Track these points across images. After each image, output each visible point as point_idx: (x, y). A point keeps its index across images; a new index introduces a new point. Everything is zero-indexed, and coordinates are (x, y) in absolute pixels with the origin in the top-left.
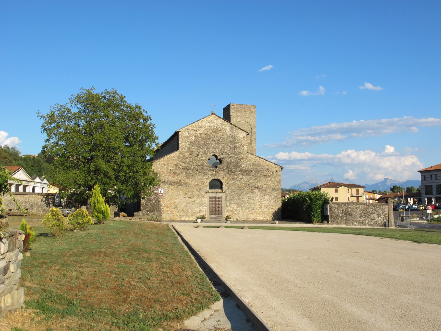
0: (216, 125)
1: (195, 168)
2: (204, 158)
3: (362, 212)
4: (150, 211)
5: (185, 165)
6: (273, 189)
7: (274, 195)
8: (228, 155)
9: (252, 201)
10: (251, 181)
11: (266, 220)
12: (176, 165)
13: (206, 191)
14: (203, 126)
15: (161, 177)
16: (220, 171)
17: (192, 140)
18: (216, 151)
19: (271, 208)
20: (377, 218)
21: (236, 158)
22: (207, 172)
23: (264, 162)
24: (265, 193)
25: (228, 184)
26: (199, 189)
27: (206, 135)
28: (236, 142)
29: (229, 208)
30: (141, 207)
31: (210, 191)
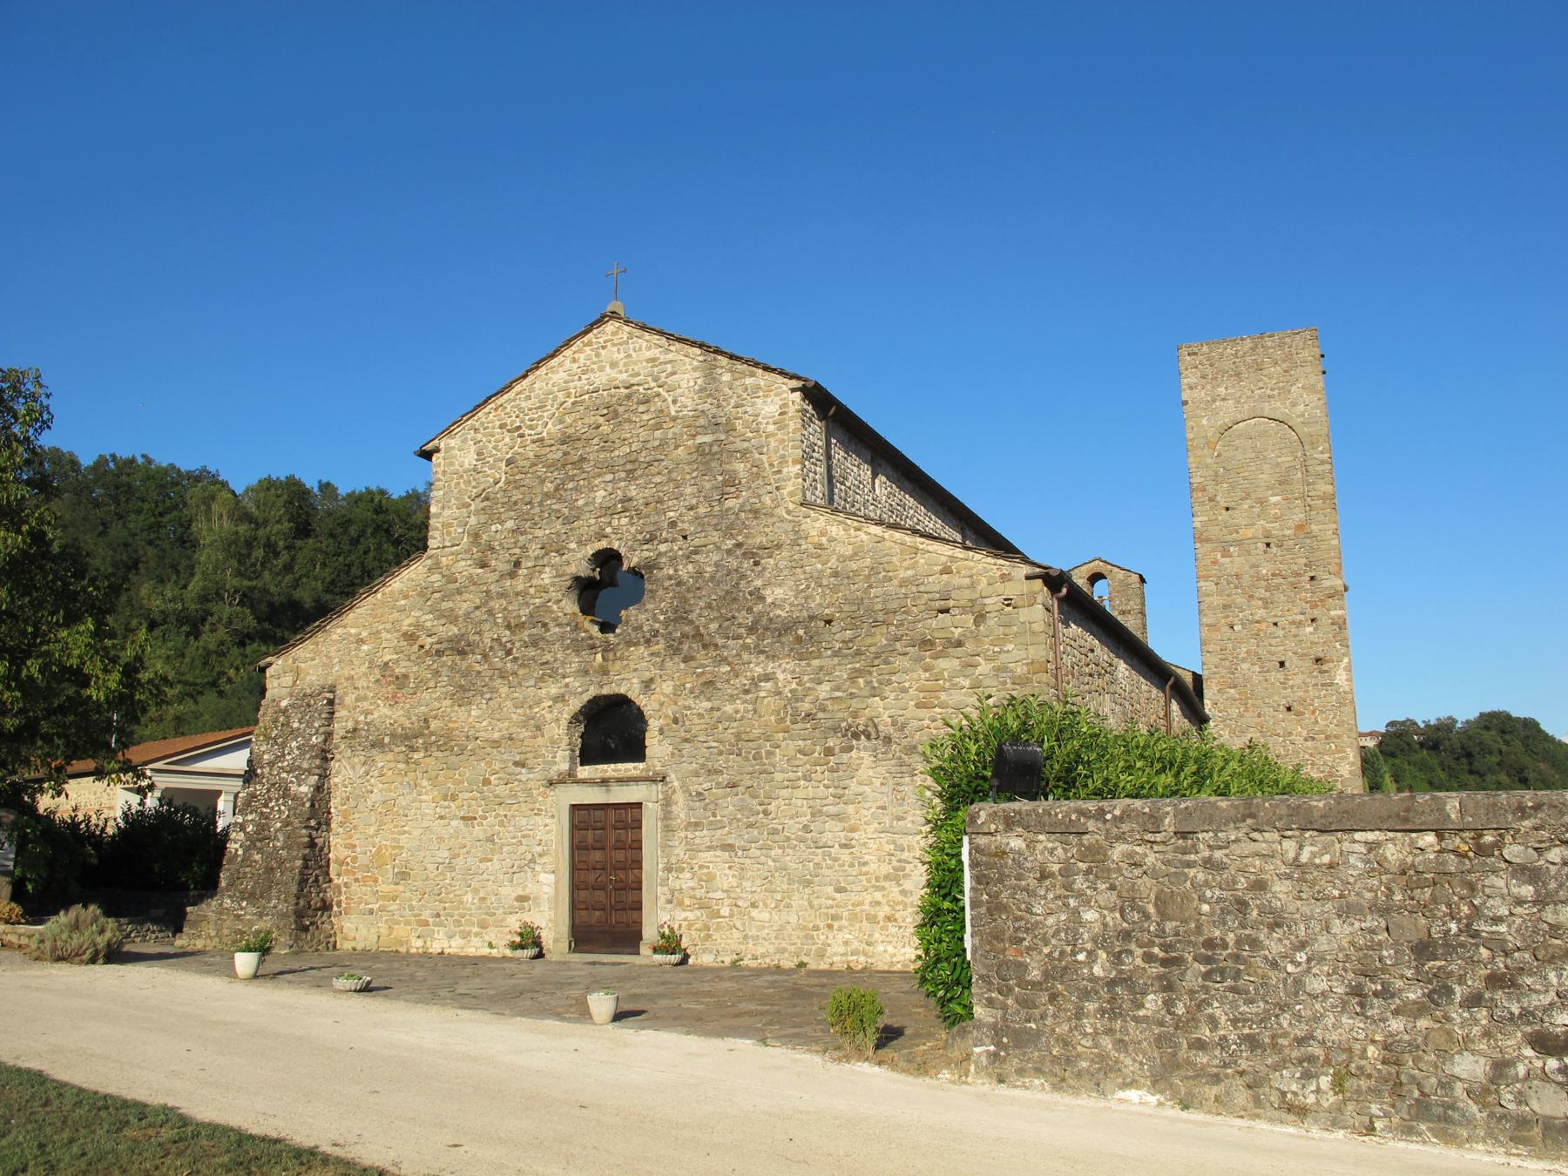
0: (624, 376)
1: (498, 640)
2: (547, 577)
3: (1371, 922)
5: (454, 630)
9: (833, 832)
10: (824, 690)
12: (410, 637)
13: (553, 773)
16: (629, 643)
18: (615, 523)
21: (729, 552)
23: (916, 550)
25: (676, 721)
26: (516, 764)
29: (685, 881)
31: (584, 772)
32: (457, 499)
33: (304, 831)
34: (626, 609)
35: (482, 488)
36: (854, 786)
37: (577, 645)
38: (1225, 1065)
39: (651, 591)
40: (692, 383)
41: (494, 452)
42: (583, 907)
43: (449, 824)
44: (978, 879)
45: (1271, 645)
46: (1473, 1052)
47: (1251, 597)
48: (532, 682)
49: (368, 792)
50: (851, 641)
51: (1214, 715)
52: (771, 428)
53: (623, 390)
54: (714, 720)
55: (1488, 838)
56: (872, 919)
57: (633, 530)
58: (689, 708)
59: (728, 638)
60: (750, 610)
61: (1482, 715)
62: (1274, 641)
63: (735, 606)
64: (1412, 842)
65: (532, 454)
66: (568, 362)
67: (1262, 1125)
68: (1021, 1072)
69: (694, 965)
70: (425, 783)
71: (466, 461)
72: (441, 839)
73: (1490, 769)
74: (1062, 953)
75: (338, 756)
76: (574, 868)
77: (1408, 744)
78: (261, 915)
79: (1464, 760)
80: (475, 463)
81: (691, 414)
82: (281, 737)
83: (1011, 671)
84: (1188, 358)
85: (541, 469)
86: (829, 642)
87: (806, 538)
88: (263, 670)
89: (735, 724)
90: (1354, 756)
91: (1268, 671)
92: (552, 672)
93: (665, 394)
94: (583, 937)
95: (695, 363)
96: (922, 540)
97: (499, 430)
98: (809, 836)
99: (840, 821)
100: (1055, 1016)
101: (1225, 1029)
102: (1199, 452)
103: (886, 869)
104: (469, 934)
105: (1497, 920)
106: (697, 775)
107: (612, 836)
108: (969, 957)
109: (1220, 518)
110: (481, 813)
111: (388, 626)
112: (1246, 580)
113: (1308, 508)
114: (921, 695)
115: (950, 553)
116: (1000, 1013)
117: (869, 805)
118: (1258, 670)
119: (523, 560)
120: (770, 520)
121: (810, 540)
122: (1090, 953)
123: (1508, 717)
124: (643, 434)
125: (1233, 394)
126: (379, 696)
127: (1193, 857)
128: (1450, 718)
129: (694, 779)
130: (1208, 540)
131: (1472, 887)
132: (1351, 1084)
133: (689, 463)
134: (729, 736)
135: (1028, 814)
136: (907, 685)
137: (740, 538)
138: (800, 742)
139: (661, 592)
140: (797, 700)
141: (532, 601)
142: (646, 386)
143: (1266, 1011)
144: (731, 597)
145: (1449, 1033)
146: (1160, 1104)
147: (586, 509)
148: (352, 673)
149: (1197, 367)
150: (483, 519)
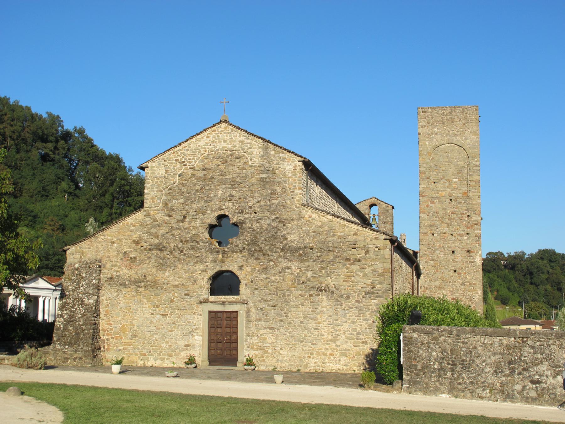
0: (230, 146)
1: (177, 246)
2: (198, 223)
3: (500, 356)
4: (70, 344)
5: (157, 241)
6: (368, 293)
7: (370, 307)
8: (256, 213)
9: (311, 324)
10: (309, 274)
11: (350, 372)
12: (137, 242)
13: (201, 298)
14: (200, 152)
15: (104, 269)
16: (233, 252)
17: (174, 183)
18: (227, 204)
19: (363, 343)
20: (551, 378)
21: (273, 220)
22: (204, 254)
23: (345, 226)
24: (346, 304)
25: (252, 282)
26: (185, 295)
27: (204, 170)
28: (274, 183)
29: (255, 340)
30: (54, 335)
31: (212, 298)
32: (157, 188)
33: (93, 318)
34: (232, 238)
35: (168, 184)
36: (320, 308)
37: (211, 251)
38: (466, 388)
39: (242, 232)
40: (258, 153)
41: (173, 171)
42: (213, 349)
43: (156, 317)
44: (405, 344)
45: (449, 244)
46: (519, 384)
47: (442, 222)
48: (192, 264)
49: (118, 303)
50: (320, 257)
51: (424, 272)
52: (290, 175)
53: (229, 152)
54: (267, 282)
55: (525, 339)
56: (325, 354)
57: (234, 208)
58: (258, 277)
59: (273, 252)
60: (282, 243)
61: (540, 251)
62: (450, 242)
63: (276, 241)
64: (509, 340)
65: (190, 173)
66: (205, 137)
67: (473, 401)
68: (415, 391)
69: (257, 370)
70: (145, 300)
71: (161, 173)
72: (152, 322)
73: (542, 282)
74: (427, 362)
75: (103, 288)
76: (210, 335)
77: (498, 266)
78: (76, 351)
79: (528, 277)
80: (164, 174)
81: (258, 165)
82: (76, 279)
83: (377, 271)
84: (422, 113)
85: (194, 180)
86: (312, 257)
87: (304, 218)
88: (65, 251)
89: (275, 284)
90: (481, 293)
91: (447, 255)
92: (201, 260)
93: (246, 156)
94: (213, 360)
95: (259, 145)
96: (347, 222)
97: (175, 162)
98: (303, 325)
99: (314, 320)
100: (424, 377)
101: (466, 380)
102: (424, 156)
103: (330, 337)
104: (164, 359)
105: (525, 357)
106: (260, 301)
107: (225, 323)
108: (402, 363)
109: (431, 186)
110: (170, 313)
111: (126, 237)
112: (441, 215)
113: (469, 185)
114: (345, 277)
115: (357, 228)
116: (410, 377)
117: (325, 315)
118: (443, 254)
119: (187, 216)
120: (290, 210)
121: (305, 218)
122: (434, 363)
123: (554, 253)
124: (238, 171)
125: (440, 132)
126: (123, 265)
127: (460, 341)
128: (522, 252)
129: (259, 303)
130: (425, 196)
131: (521, 350)
132: (493, 391)
133: (257, 184)
134: (273, 288)
135: (419, 329)
136: (340, 273)
137: (278, 215)
138: (300, 292)
139: (246, 233)
140: (299, 277)
141: (191, 232)
142: (239, 152)
143: (475, 376)
144: (274, 237)
145: (514, 380)
146: (450, 397)
147: (214, 198)
148: (109, 255)
149: (425, 118)
150: (169, 197)
